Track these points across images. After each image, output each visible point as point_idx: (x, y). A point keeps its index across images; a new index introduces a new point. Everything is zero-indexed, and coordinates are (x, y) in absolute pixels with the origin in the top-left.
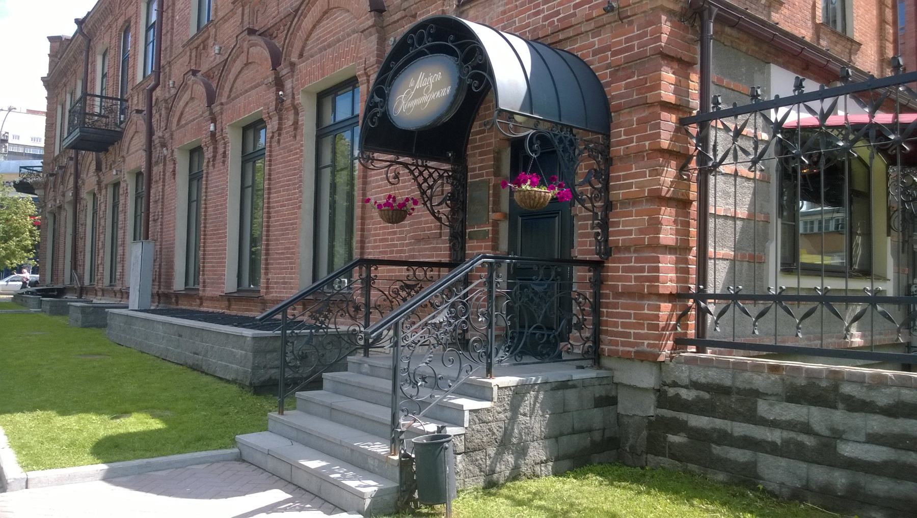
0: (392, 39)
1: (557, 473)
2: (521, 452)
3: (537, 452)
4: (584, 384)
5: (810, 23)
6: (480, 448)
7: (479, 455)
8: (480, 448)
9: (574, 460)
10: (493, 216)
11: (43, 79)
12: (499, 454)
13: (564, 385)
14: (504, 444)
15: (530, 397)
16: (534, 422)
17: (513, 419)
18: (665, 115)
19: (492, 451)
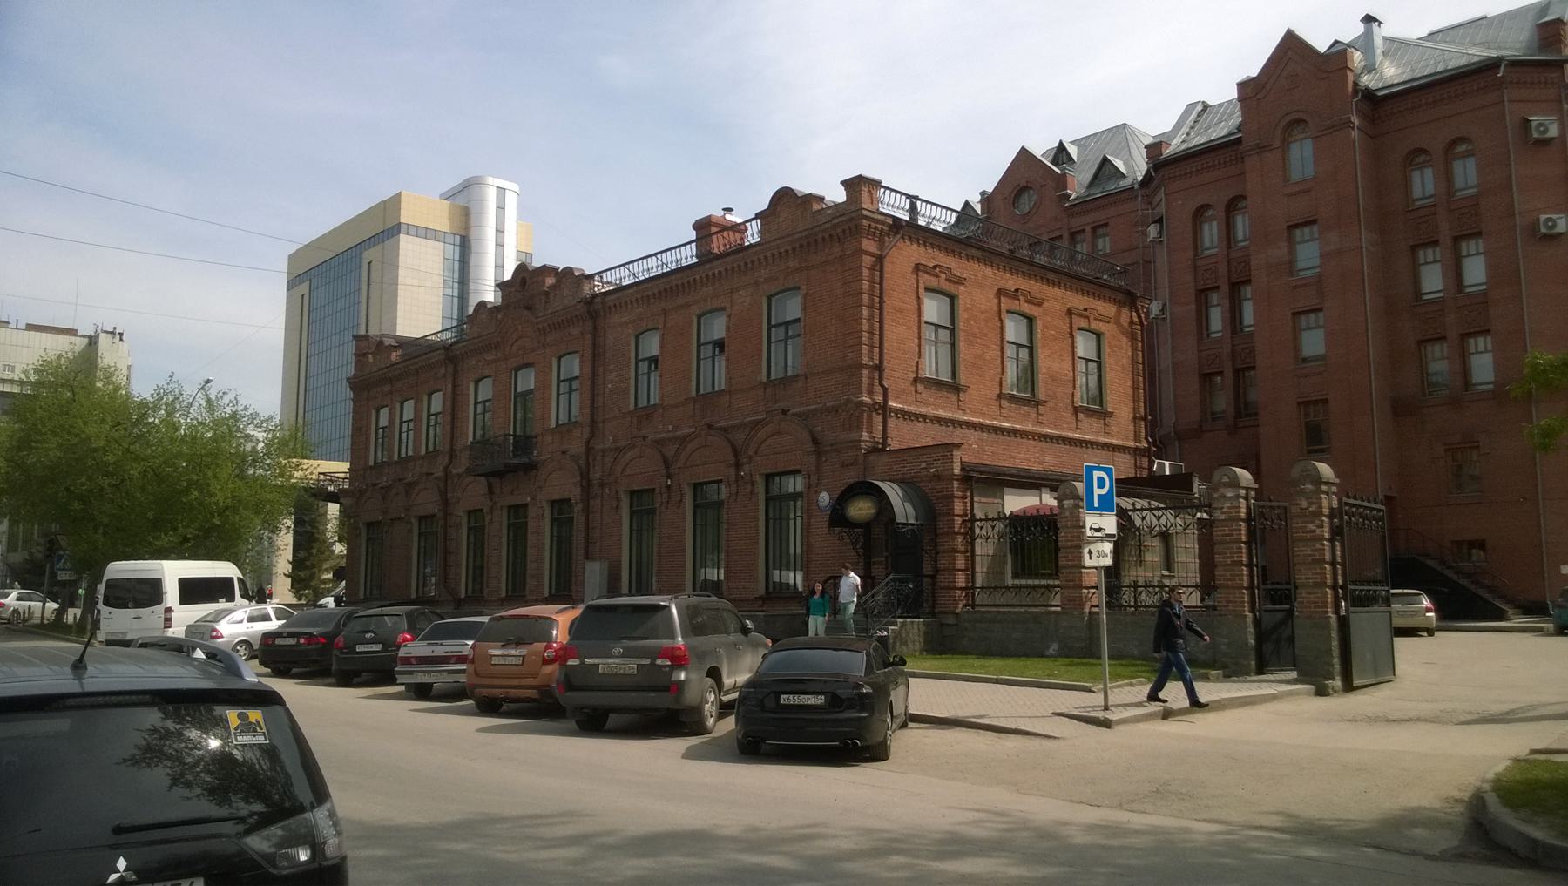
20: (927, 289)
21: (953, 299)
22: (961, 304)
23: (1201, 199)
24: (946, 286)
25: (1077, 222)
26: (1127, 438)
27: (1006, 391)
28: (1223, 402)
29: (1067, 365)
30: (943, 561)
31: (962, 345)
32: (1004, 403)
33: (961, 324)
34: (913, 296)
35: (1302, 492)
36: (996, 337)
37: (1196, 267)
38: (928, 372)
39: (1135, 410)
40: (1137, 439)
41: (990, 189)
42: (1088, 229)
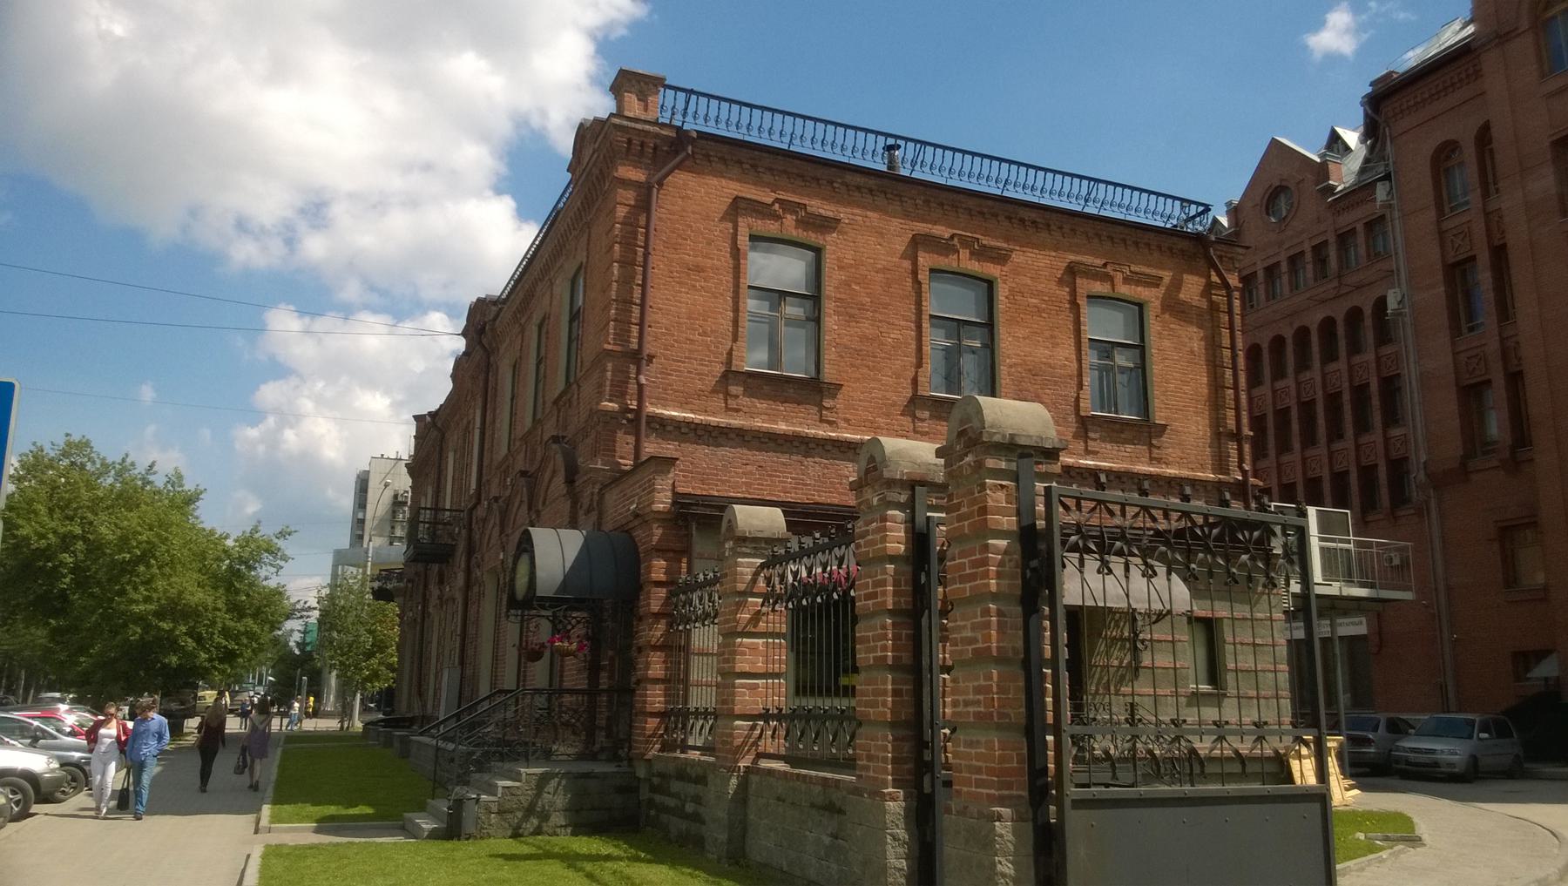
0: (1402, 16)
1: (574, 834)
2: (545, 817)
3: (557, 819)
4: (605, 776)
5: (1072, 418)
6: (511, 811)
7: (509, 816)
8: (511, 811)
9: (588, 821)
10: (610, 653)
11: (191, 499)
12: (526, 817)
13: (587, 776)
14: (530, 811)
15: (554, 783)
16: (556, 798)
17: (538, 795)
18: (662, 577)
19: (519, 814)
20: (1093, 298)
21: (818, 251)
22: (1002, 293)
23: (1438, 137)
24: (974, 267)
25: (1346, 220)
26: (1202, 467)
27: (925, 391)
28: (1496, 426)
29: (1066, 351)
30: (629, 666)
31: (830, 322)
32: (735, 389)
33: (829, 289)
34: (727, 246)
35: (221, 694)
36: (909, 310)
37: (1441, 234)
38: (754, 359)
39: (1217, 423)
40: (1221, 465)
41: (1236, 199)
42: (1360, 227)
